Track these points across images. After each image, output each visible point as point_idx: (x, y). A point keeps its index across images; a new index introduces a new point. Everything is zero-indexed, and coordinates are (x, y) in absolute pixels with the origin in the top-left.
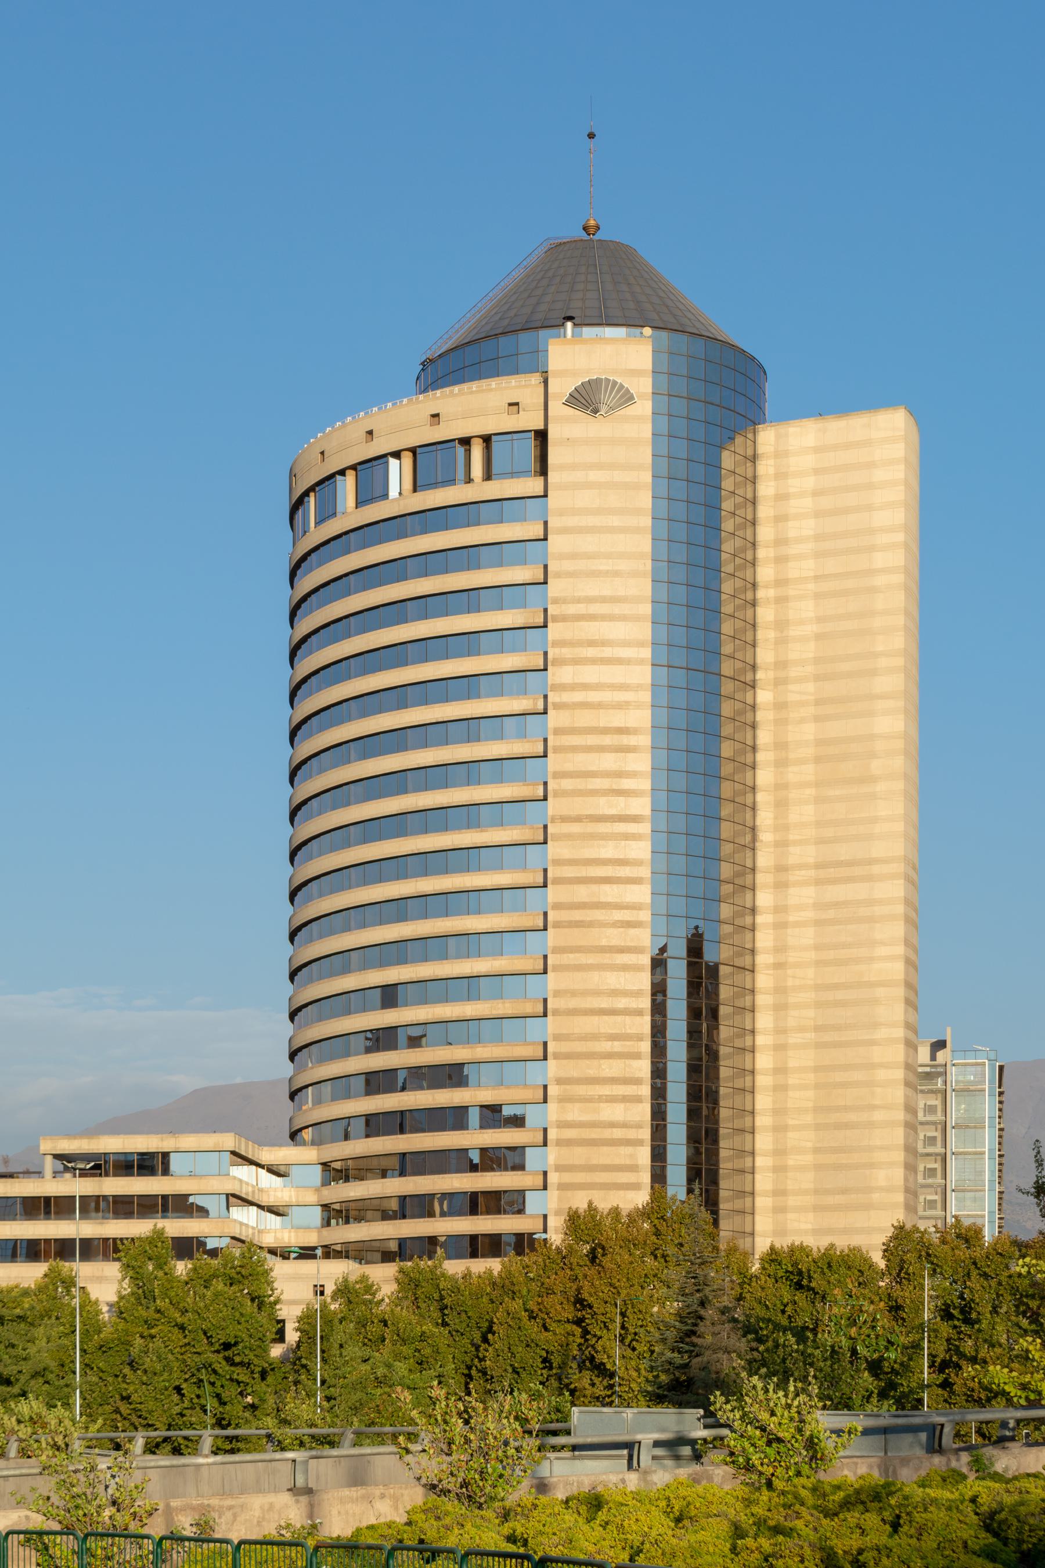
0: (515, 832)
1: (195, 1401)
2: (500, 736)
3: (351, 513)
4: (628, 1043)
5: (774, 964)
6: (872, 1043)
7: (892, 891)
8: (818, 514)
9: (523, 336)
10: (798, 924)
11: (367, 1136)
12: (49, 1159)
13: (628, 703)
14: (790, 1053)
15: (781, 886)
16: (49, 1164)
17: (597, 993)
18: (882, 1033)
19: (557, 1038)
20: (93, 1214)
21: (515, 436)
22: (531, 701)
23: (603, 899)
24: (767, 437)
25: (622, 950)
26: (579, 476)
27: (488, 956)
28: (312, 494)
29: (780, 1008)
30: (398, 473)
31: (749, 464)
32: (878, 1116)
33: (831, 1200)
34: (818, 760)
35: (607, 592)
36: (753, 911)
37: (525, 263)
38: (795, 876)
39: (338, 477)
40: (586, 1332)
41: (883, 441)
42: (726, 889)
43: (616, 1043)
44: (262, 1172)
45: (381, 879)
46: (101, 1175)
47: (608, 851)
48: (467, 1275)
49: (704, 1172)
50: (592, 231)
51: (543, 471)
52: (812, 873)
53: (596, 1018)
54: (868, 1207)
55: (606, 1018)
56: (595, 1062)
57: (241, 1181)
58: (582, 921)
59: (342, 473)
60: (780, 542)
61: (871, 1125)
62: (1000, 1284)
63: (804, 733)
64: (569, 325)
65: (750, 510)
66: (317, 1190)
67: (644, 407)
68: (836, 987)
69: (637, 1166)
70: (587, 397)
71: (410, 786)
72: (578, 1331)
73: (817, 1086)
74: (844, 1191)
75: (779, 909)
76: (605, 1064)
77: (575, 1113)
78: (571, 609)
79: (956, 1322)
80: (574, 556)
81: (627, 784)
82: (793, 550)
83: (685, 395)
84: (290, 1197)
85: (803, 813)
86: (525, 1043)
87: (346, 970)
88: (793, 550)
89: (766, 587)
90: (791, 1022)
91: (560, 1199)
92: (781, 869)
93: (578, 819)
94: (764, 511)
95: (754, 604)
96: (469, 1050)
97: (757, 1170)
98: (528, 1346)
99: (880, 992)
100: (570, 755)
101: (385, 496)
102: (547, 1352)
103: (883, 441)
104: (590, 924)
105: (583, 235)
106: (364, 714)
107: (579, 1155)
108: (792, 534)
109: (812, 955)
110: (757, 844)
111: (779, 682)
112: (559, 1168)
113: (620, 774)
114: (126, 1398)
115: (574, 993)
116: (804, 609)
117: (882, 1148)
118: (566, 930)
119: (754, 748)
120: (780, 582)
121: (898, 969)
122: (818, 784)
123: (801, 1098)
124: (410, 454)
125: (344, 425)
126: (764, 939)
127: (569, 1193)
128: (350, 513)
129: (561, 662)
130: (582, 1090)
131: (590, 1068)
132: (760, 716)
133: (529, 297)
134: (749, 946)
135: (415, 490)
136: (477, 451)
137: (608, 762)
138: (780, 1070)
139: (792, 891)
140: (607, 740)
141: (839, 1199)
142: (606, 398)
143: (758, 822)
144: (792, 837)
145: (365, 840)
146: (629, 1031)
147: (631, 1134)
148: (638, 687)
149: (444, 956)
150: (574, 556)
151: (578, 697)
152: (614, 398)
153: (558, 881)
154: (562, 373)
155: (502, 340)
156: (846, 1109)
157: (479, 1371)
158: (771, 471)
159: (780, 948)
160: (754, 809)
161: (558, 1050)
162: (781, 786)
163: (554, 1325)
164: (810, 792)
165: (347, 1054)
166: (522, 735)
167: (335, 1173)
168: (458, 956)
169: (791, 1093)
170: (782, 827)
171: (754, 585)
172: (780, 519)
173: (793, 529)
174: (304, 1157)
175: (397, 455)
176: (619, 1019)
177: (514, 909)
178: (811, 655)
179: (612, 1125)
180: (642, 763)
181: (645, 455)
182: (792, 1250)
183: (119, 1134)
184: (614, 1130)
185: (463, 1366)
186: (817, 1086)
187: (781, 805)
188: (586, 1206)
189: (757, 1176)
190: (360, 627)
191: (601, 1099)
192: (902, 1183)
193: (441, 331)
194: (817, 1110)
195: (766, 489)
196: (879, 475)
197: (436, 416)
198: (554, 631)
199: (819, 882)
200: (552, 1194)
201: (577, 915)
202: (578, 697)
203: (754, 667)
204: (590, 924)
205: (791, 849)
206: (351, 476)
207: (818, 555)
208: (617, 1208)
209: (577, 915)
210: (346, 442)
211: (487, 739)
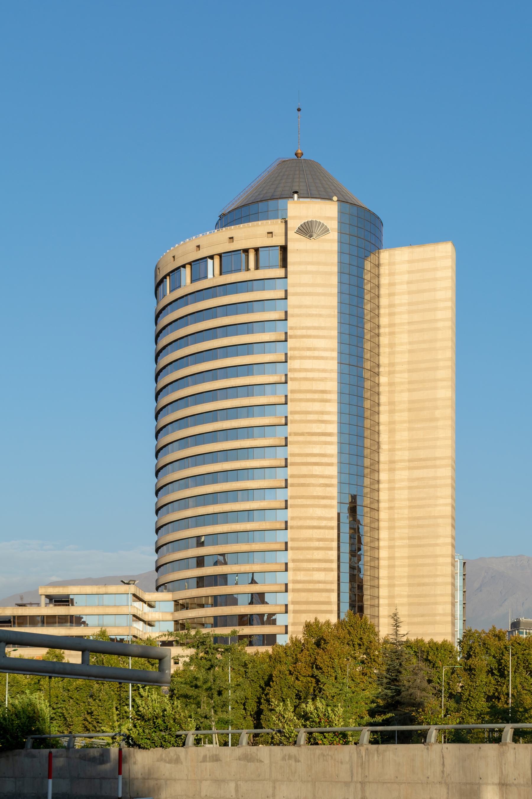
0: (271, 440)
1: (124, 714)
2: (263, 394)
3: (189, 286)
4: (326, 543)
5: (388, 507)
6: (436, 545)
7: (445, 473)
8: (410, 293)
9: (271, 203)
10: (400, 488)
11: (197, 587)
12: (43, 597)
13: (326, 378)
14: (396, 550)
15: (392, 470)
16: (43, 600)
17: (312, 518)
18: (441, 541)
19: (293, 540)
20: (57, 625)
21: (271, 248)
22: (279, 377)
23: (314, 473)
24: (385, 255)
25: (324, 498)
26: (302, 268)
27: (257, 500)
28: (168, 277)
29: (391, 528)
30: (213, 267)
31: (377, 268)
32: (439, 580)
33: (416, 620)
34: (409, 410)
35: (316, 324)
36: (378, 482)
37: (268, 169)
38: (398, 465)
39: (182, 269)
40: (318, 681)
41: (439, 260)
42: (367, 471)
43: (321, 543)
44: (146, 606)
45: (204, 463)
46: (69, 605)
47: (317, 450)
48: (257, 654)
49: (357, 604)
50: (299, 156)
51: (284, 264)
52: (407, 464)
53: (311, 530)
54: (434, 623)
55: (316, 530)
56: (311, 552)
57: (137, 608)
58: (305, 484)
59: (184, 266)
60: (391, 306)
61: (435, 584)
62: (518, 658)
63: (403, 397)
64: (296, 195)
65: (377, 290)
66: (172, 613)
67: (334, 235)
68: (418, 518)
69: (331, 602)
70: (306, 230)
71: (219, 418)
72: (314, 680)
73: (409, 566)
74: (422, 616)
75: (391, 481)
76: (316, 552)
77: (301, 576)
78: (299, 332)
79: (496, 677)
80: (300, 307)
81: (326, 417)
82: (398, 310)
83: (348, 233)
84: (159, 617)
85: (402, 435)
86: (276, 543)
87: (187, 507)
88: (398, 310)
89: (385, 327)
90: (397, 535)
91: (294, 618)
92: (392, 462)
93: (302, 434)
94: (383, 291)
95: (378, 335)
96: (249, 546)
97: (380, 605)
98: (289, 688)
99: (440, 521)
100: (298, 403)
101: (206, 277)
102: (298, 691)
103: (439, 260)
104: (308, 485)
105: (296, 157)
106: (195, 383)
107: (303, 597)
108: (397, 302)
109: (407, 503)
110: (380, 450)
111: (390, 373)
112: (293, 603)
113: (322, 413)
114: (91, 713)
115: (300, 518)
116: (403, 338)
117: (441, 595)
118: (297, 488)
119: (379, 404)
120: (391, 325)
121: (448, 510)
122: (409, 422)
123: (401, 571)
124: (218, 257)
125: (185, 243)
126: (383, 496)
127: (298, 615)
128: (188, 285)
129: (294, 358)
130: (305, 565)
131: (309, 555)
132: (381, 389)
133: (272, 184)
134: (377, 499)
135: (221, 274)
136: (252, 256)
137: (317, 407)
138: (392, 558)
139: (397, 472)
140: (316, 396)
141: (420, 619)
142: (317, 231)
143: (381, 440)
144: (397, 446)
145: (196, 444)
146: (327, 537)
147: (328, 587)
148: (332, 371)
149: (236, 500)
150: (300, 307)
151: (302, 375)
152: (320, 230)
153: (293, 464)
154: (294, 218)
155: (260, 204)
156: (423, 576)
157: (265, 700)
158: (387, 272)
159: (391, 500)
160: (378, 433)
161: (293, 546)
162: (392, 423)
163: (302, 678)
164: (406, 425)
165: (187, 548)
166: (274, 393)
167: (180, 606)
168: (243, 500)
169: (396, 569)
170: (392, 442)
171: (379, 326)
172: (391, 295)
173: (397, 300)
174: (165, 597)
175: (212, 257)
176: (322, 531)
177: (270, 478)
178: (406, 360)
179: (319, 582)
180: (333, 407)
181: (335, 258)
182: (417, 641)
183: (78, 585)
184: (320, 584)
185: (256, 698)
186: (409, 566)
187: (392, 431)
188: (314, 621)
189: (381, 609)
190: (189, 345)
191: (314, 570)
192: (450, 612)
193: (229, 201)
194: (409, 577)
195: (384, 280)
196: (439, 274)
197: (232, 238)
198: (291, 343)
199: (410, 468)
200: (290, 615)
201: (302, 481)
202: (302, 375)
203: (378, 366)
204: (308, 485)
205: (397, 453)
206: (188, 268)
207: (410, 312)
208: (329, 621)
209: (302, 481)
210: (186, 251)
211: (257, 395)
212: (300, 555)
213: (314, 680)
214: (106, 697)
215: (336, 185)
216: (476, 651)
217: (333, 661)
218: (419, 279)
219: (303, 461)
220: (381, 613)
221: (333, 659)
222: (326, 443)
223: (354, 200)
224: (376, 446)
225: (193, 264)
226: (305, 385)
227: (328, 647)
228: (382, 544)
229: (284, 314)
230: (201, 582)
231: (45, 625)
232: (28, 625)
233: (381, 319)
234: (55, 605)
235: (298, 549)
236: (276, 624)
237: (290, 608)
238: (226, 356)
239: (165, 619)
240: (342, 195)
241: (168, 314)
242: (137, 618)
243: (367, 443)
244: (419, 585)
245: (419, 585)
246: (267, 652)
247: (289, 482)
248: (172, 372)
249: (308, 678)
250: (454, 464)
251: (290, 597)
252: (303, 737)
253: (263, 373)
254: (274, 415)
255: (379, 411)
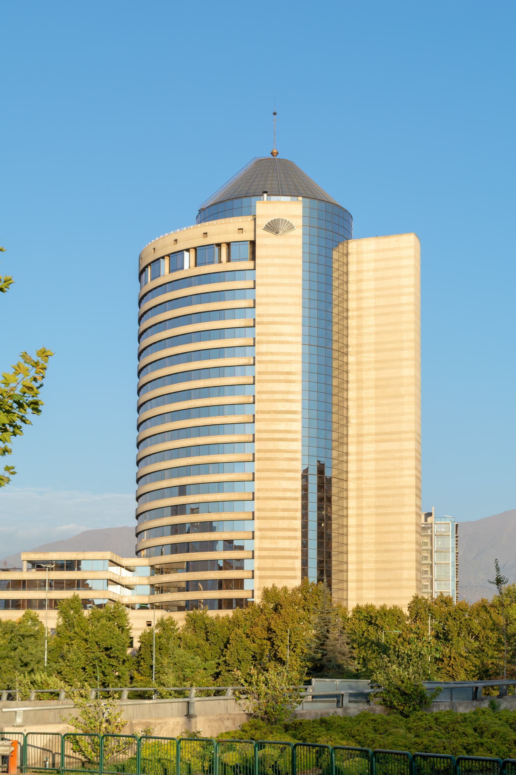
2: (233, 375)
4: (291, 513)
6: (402, 513)
9: (245, 200)
12: (25, 563)
13: (291, 361)
15: (359, 443)
16: (25, 565)
17: (277, 490)
18: (406, 509)
19: (259, 510)
20: (38, 588)
21: (241, 243)
23: (280, 448)
24: (353, 245)
25: (288, 471)
28: (149, 267)
29: (359, 497)
30: (188, 258)
31: (345, 257)
33: (382, 584)
34: (376, 387)
39: (161, 260)
42: (335, 444)
43: (285, 513)
44: (123, 570)
47: (282, 426)
48: (217, 618)
49: (325, 571)
51: (253, 258)
53: (277, 501)
55: (281, 501)
56: (276, 521)
57: (113, 573)
59: (163, 258)
62: (461, 623)
64: (265, 195)
66: (148, 578)
67: (299, 231)
69: (295, 568)
74: (389, 580)
76: (281, 522)
77: (267, 544)
78: (266, 319)
80: (268, 296)
81: (291, 397)
86: (244, 512)
87: (163, 478)
89: (353, 311)
93: (269, 412)
95: (347, 318)
98: (245, 650)
101: (182, 268)
102: (255, 653)
104: (274, 459)
106: (172, 364)
107: (269, 563)
110: (349, 424)
111: (358, 353)
112: (259, 569)
115: (266, 490)
119: (347, 382)
121: (412, 481)
124: (194, 250)
125: (164, 237)
126: (352, 467)
127: (264, 580)
128: (166, 275)
131: (274, 524)
132: (350, 367)
133: (247, 182)
137: (283, 387)
140: (282, 377)
141: (386, 584)
142: (282, 227)
143: (349, 415)
147: (293, 554)
148: (296, 354)
149: (207, 473)
150: (268, 296)
153: (260, 440)
155: (235, 201)
156: (389, 543)
158: (355, 260)
159: (359, 471)
160: (347, 409)
162: (359, 399)
165: (162, 516)
166: (244, 374)
168: (214, 473)
171: (347, 310)
172: (359, 281)
174: (142, 563)
175: (188, 250)
177: (240, 452)
179: (284, 550)
180: (298, 387)
182: (367, 607)
184: (285, 552)
187: (360, 407)
188: (272, 586)
189: (349, 573)
191: (279, 538)
195: (352, 268)
197: (205, 234)
198: (258, 329)
199: (377, 441)
200: (256, 580)
201: (268, 455)
204: (274, 459)
206: (167, 259)
209: (268, 455)
210: (165, 245)
211: (227, 376)
212: (266, 524)
213: (269, 643)
214: (75, 658)
215: (306, 183)
216: (422, 616)
217: (286, 625)
218: (384, 269)
219: (269, 437)
220: (349, 578)
221: (287, 623)
222: (291, 420)
223: (322, 196)
224: (345, 421)
225: (171, 255)
226: (272, 368)
227: (282, 611)
228: (350, 512)
229: (253, 302)
230: (176, 548)
231: (26, 588)
232: (10, 589)
233: (349, 303)
234: (37, 570)
235: (264, 518)
236: (243, 589)
237: (257, 573)
238: (200, 340)
239: (141, 583)
240: (312, 192)
241: (148, 300)
242: (111, 582)
243: (335, 418)
244: (386, 551)
245: (386, 551)
246: (228, 616)
247: (256, 456)
248: (152, 353)
249: (264, 641)
250: (418, 438)
251: (256, 563)
252: (33, 696)
253: (234, 356)
254: (244, 394)
255: (347, 388)
